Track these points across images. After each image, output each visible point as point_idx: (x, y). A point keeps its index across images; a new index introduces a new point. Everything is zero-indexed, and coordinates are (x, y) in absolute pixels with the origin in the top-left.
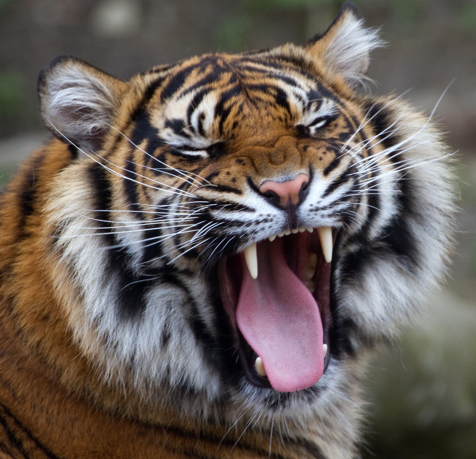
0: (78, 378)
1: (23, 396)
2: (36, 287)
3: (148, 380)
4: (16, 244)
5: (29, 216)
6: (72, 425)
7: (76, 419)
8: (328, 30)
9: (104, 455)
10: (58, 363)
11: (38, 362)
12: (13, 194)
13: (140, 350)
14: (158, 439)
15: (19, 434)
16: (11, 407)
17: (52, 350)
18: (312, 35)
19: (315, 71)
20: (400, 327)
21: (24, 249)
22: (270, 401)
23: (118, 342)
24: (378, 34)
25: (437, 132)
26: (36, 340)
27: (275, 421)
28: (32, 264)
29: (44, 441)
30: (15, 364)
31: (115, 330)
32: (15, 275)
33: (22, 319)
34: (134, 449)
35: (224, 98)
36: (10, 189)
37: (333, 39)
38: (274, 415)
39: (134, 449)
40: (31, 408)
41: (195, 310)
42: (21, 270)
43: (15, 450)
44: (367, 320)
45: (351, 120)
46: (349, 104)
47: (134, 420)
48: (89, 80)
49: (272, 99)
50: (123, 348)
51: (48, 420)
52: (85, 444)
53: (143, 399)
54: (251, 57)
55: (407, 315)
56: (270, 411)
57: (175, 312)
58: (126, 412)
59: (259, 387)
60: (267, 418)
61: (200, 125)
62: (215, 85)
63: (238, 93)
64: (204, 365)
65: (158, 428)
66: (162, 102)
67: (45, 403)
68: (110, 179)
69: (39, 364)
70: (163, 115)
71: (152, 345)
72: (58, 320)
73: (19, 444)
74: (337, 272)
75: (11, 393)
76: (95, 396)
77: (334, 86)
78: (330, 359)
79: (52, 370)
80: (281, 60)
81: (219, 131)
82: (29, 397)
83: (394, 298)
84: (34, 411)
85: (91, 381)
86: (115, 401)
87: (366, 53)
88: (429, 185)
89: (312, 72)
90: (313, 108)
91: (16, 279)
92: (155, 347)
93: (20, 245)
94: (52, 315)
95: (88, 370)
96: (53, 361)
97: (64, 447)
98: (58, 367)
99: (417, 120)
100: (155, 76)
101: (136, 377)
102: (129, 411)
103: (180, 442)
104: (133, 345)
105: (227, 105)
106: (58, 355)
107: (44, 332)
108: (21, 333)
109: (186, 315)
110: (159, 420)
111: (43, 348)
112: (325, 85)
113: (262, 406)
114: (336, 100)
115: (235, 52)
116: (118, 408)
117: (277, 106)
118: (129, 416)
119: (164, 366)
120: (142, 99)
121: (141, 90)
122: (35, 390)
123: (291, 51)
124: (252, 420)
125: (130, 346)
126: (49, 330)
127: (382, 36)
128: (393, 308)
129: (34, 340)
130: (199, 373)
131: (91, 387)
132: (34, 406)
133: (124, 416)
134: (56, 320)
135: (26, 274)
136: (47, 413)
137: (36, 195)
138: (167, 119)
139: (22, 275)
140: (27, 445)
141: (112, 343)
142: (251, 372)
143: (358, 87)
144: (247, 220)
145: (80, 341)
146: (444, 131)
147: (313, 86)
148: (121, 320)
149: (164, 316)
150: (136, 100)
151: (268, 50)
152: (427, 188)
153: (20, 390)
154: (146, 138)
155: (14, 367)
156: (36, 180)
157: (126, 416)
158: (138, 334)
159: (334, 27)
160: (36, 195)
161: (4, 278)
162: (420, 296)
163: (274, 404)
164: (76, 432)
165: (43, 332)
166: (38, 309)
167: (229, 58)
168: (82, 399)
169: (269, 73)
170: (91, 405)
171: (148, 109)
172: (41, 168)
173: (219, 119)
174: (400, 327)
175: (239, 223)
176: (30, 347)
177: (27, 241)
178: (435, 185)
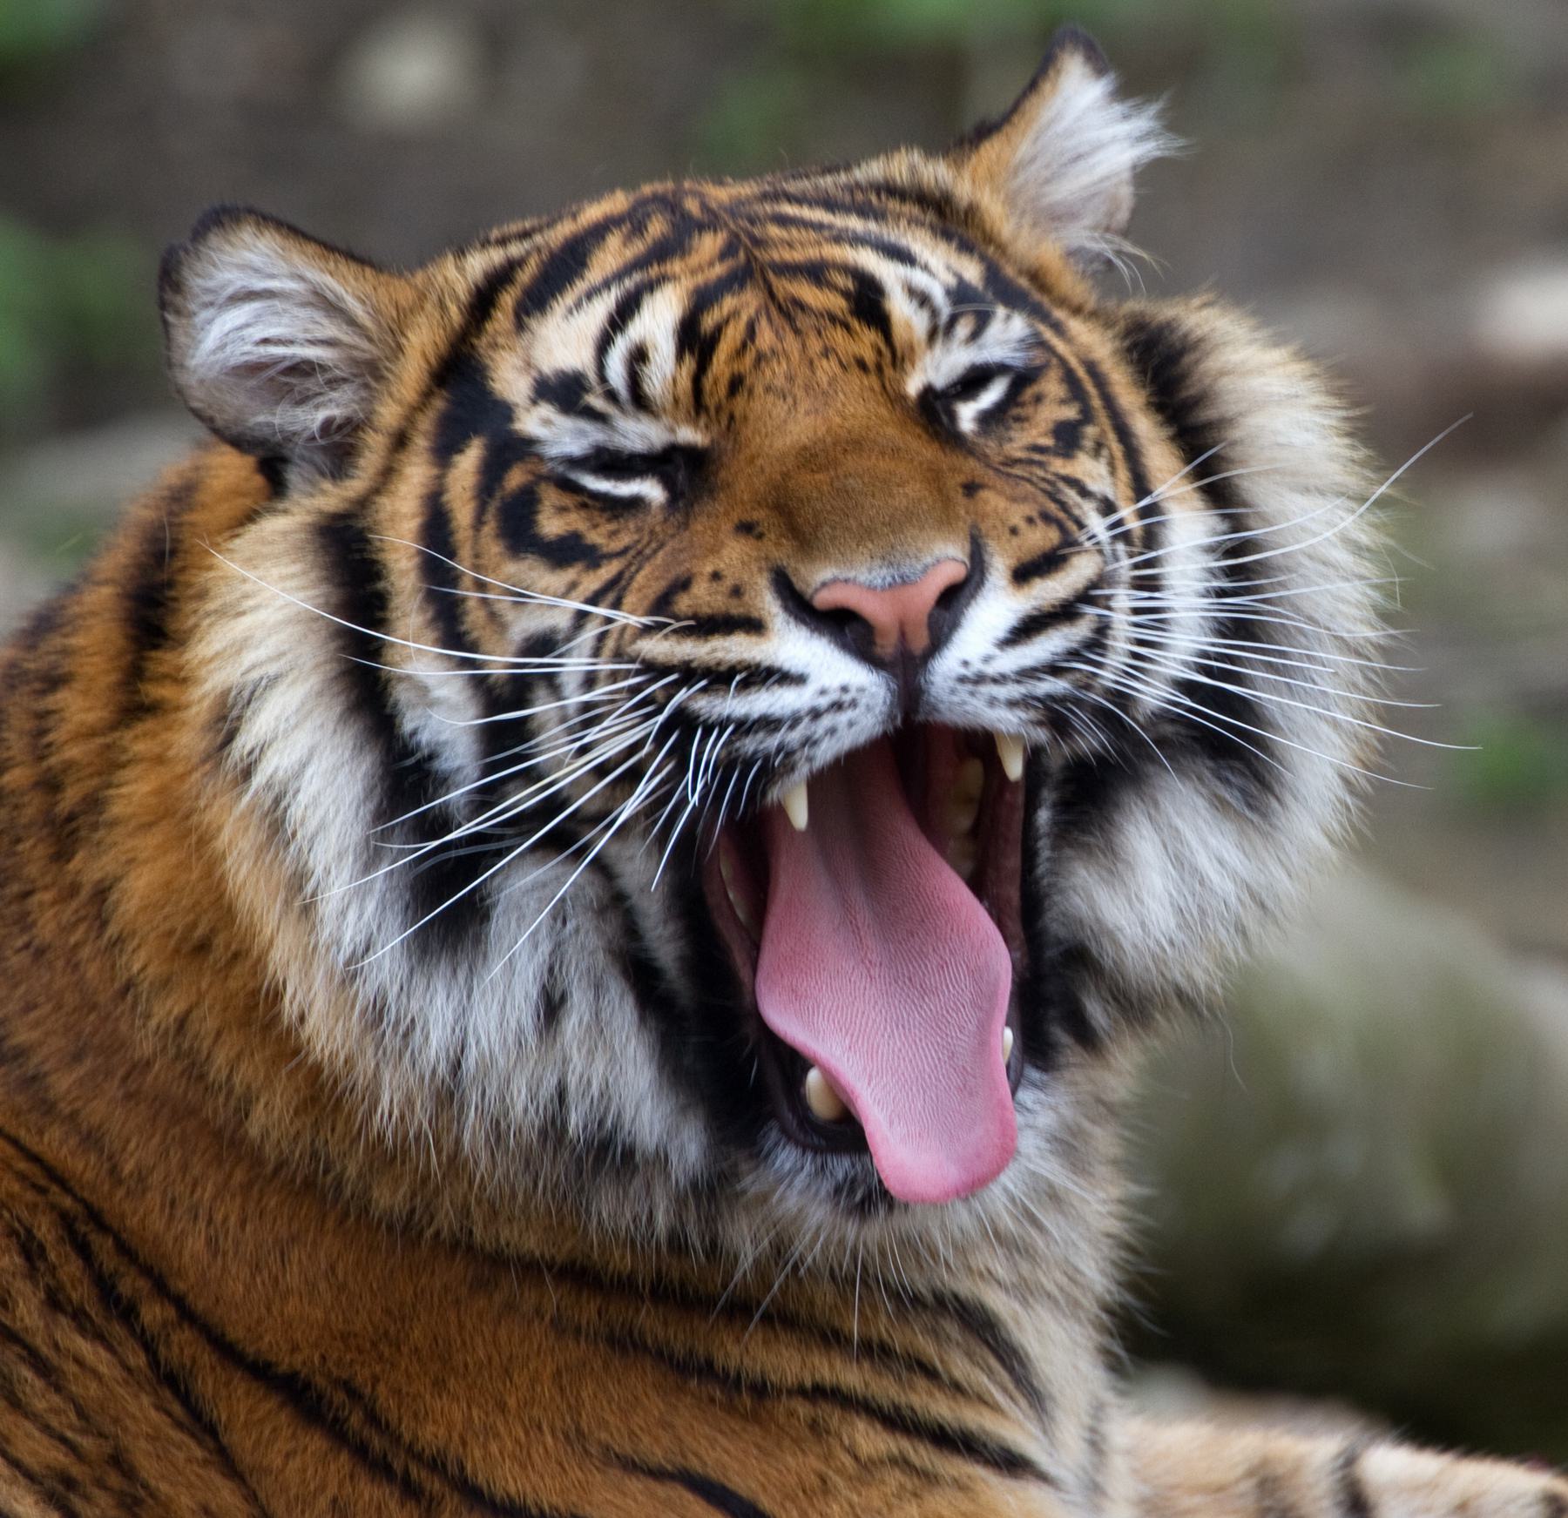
0: (298, 1124)
1: (140, 1173)
2: (172, 858)
3: (503, 1125)
4: (117, 734)
5: (153, 654)
6: (282, 1254)
7: (293, 1239)
8: (1015, 107)
9: (374, 1344)
10: (237, 1080)
11: (182, 1073)
12: (106, 591)
13: (478, 1043)
14: (529, 1299)
15: (130, 1284)
16: (106, 1206)
17: (221, 1041)
18: (968, 124)
19: (984, 231)
20: (1224, 963)
21: (140, 747)
22: (852, 1191)
23: (413, 1020)
24: (1160, 116)
25: (1335, 408)
26: (176, 1011)
27: (865, 1244)
28: (162, 791)
29: (200, 1305)
30: (116, 1082)
31: (405, 988)
32: (113, 824)
33: (134, 951)
34: (461, 1327)
35: (701, 301)
36: (102, 576)
37: (1031, 135)
38: (863, 1233)
39: (461, 1327)
40: (163, 1206)
41: (631, 929)
42: (129, 810)
43: (117, 1330)
44: (1127, 946)
45: (1081, 373)
46: (1076, 326)
47: (460, 1246)
49: (838, 304)
50: (427, 1038)
51: (212, 1244)
52: (319, 1314)
53: (482, 1178)
54: (793, 187)
55: (1242, 931)
56: (850, 1224)
57: (577, 931)
58: (436, 1221)
59: (816, 1151)
60: (841, 1242)
61: (635, 381)
62: (676, 266)
63: (742, 286)
64: (661, 1086)
65: (530, 1268)
66: (520, 326)
67: (203, 1194)
68: (381, 556)
69: (184, 1081)
70: (529, 364)
71: (513, 1024)
72: (236, 956)
73: (128, 1313)
74: (1044, 816)
75: (106, 1166)
76: (348, 1174)
77: (1037, 277)
78: (1022, 1068)
79: (221, 1100)
80: (883, 197)
81: (691, 399)
82: (156, 1178)
83: (1202, 883)
84: (171, 1217)
85: (333, 1130)
86: (401, 1192)
87: (1126, 175)
88: (1306, 562)
89: (971, 234)
90: (963, 329)
91: (118, 833)
92: (521, 1031)
93: (126, 736)
94: (219, 941)
95: (324, 1100)
96: (224, 1074)
97: (259, 1322)
98: (239, 1090)
99: (1281, 370)
100: (496, 256)
101: (467, 1116)
102: (446, 1218)
103: (593, 1307)
104: (457, 1030)
105: (709, 321)
106: (239, 1056)
107: (199, 989)
108: (132, 990)
109: (610, 942)
110: (532, 1243)
111: (196, 1036)
112: (1009, 271)
113: (828, 1207)
114: (1037, 312)
115: (742, 175)
116: (412, 1211)
117: (855, 324)
118: (445, 1233)
119: (550, 1083)
120: (461, 326)
121: (458, 299)
122: (175, 1157)
123: (913, 169)
124: (799, 1247)
125: (449, 1030)
126: (210, 985)
127: (1172, 123)
128: (1202, 911)
129: (170, 1012)
130: (647, 1107)
131: (333, 1150)
132: (173, 1204)
133: (429, 1233)
134: (229, 954)
135: (146, 819)
136: (210, 1221)
137: (173, 593)
138: (540, 372)
139: (133, 824)
140: (153, 1313)
141: (397, 1022)
142: (793, 1110)
143: (1104, 271)
144: (787, 711)
145: (302, 1019)
146: (1355, 404)
147: (972, 272)
148: (421, 960)
149: (547, 941)
150: (445, 330)
151: (848, 168)
152: (1302, 571)
153: (132, 1155)
154: (476, 432)
155: (113, 1089)
156: (173, 552)
157: (437, 1234)
158: (469, 997)
159: (1034, 100)
160: (173, 593)
161: (83, 833)
162: (1283, 884)
163: (862, 1202)
164: (293, 1278)
165: (194, 989)
166: (180, 924)
167: (720, 195)
168: (309, 1184)
169: (834, 233)
170: (336, 1200)
171: (482, 351)
172: (187, 518)
173: (690, 363)
174: (1224, 963)
175: (769, 724)
176: (156, 1033)
177: (149, 724)
178: (1325, 563)
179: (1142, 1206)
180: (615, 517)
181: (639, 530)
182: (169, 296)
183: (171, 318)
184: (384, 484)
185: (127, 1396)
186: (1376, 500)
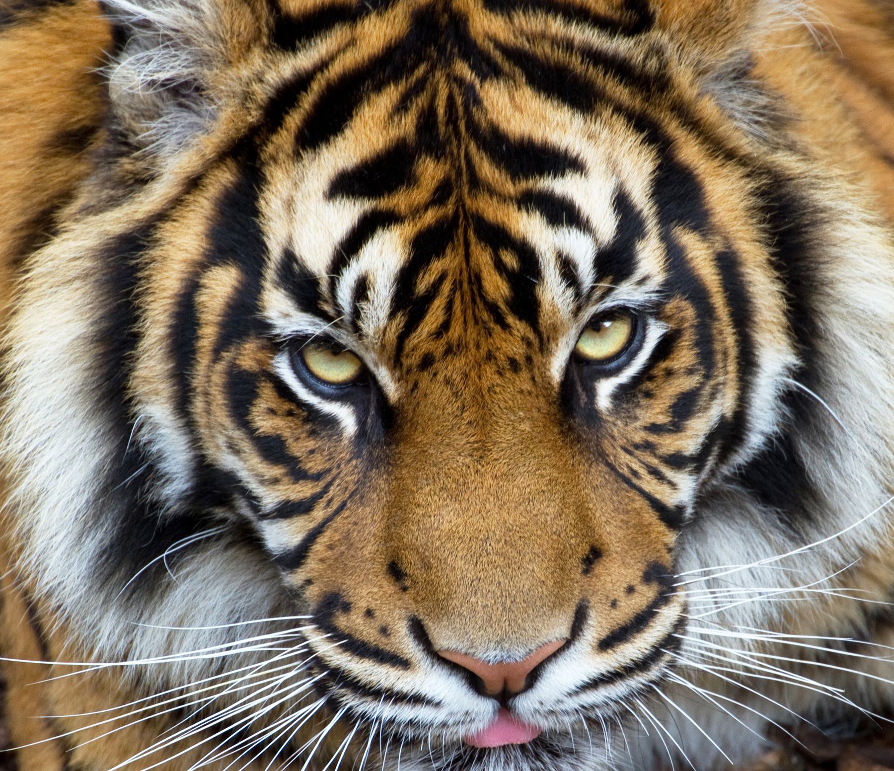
62: (400, 201)
66: (297, 156)
68: (366, 58)
173: (400, 320)
179: (704, 205)
180: (312, 433)
184: (197, 275)
185: (66, 644)
186: (846, 587)
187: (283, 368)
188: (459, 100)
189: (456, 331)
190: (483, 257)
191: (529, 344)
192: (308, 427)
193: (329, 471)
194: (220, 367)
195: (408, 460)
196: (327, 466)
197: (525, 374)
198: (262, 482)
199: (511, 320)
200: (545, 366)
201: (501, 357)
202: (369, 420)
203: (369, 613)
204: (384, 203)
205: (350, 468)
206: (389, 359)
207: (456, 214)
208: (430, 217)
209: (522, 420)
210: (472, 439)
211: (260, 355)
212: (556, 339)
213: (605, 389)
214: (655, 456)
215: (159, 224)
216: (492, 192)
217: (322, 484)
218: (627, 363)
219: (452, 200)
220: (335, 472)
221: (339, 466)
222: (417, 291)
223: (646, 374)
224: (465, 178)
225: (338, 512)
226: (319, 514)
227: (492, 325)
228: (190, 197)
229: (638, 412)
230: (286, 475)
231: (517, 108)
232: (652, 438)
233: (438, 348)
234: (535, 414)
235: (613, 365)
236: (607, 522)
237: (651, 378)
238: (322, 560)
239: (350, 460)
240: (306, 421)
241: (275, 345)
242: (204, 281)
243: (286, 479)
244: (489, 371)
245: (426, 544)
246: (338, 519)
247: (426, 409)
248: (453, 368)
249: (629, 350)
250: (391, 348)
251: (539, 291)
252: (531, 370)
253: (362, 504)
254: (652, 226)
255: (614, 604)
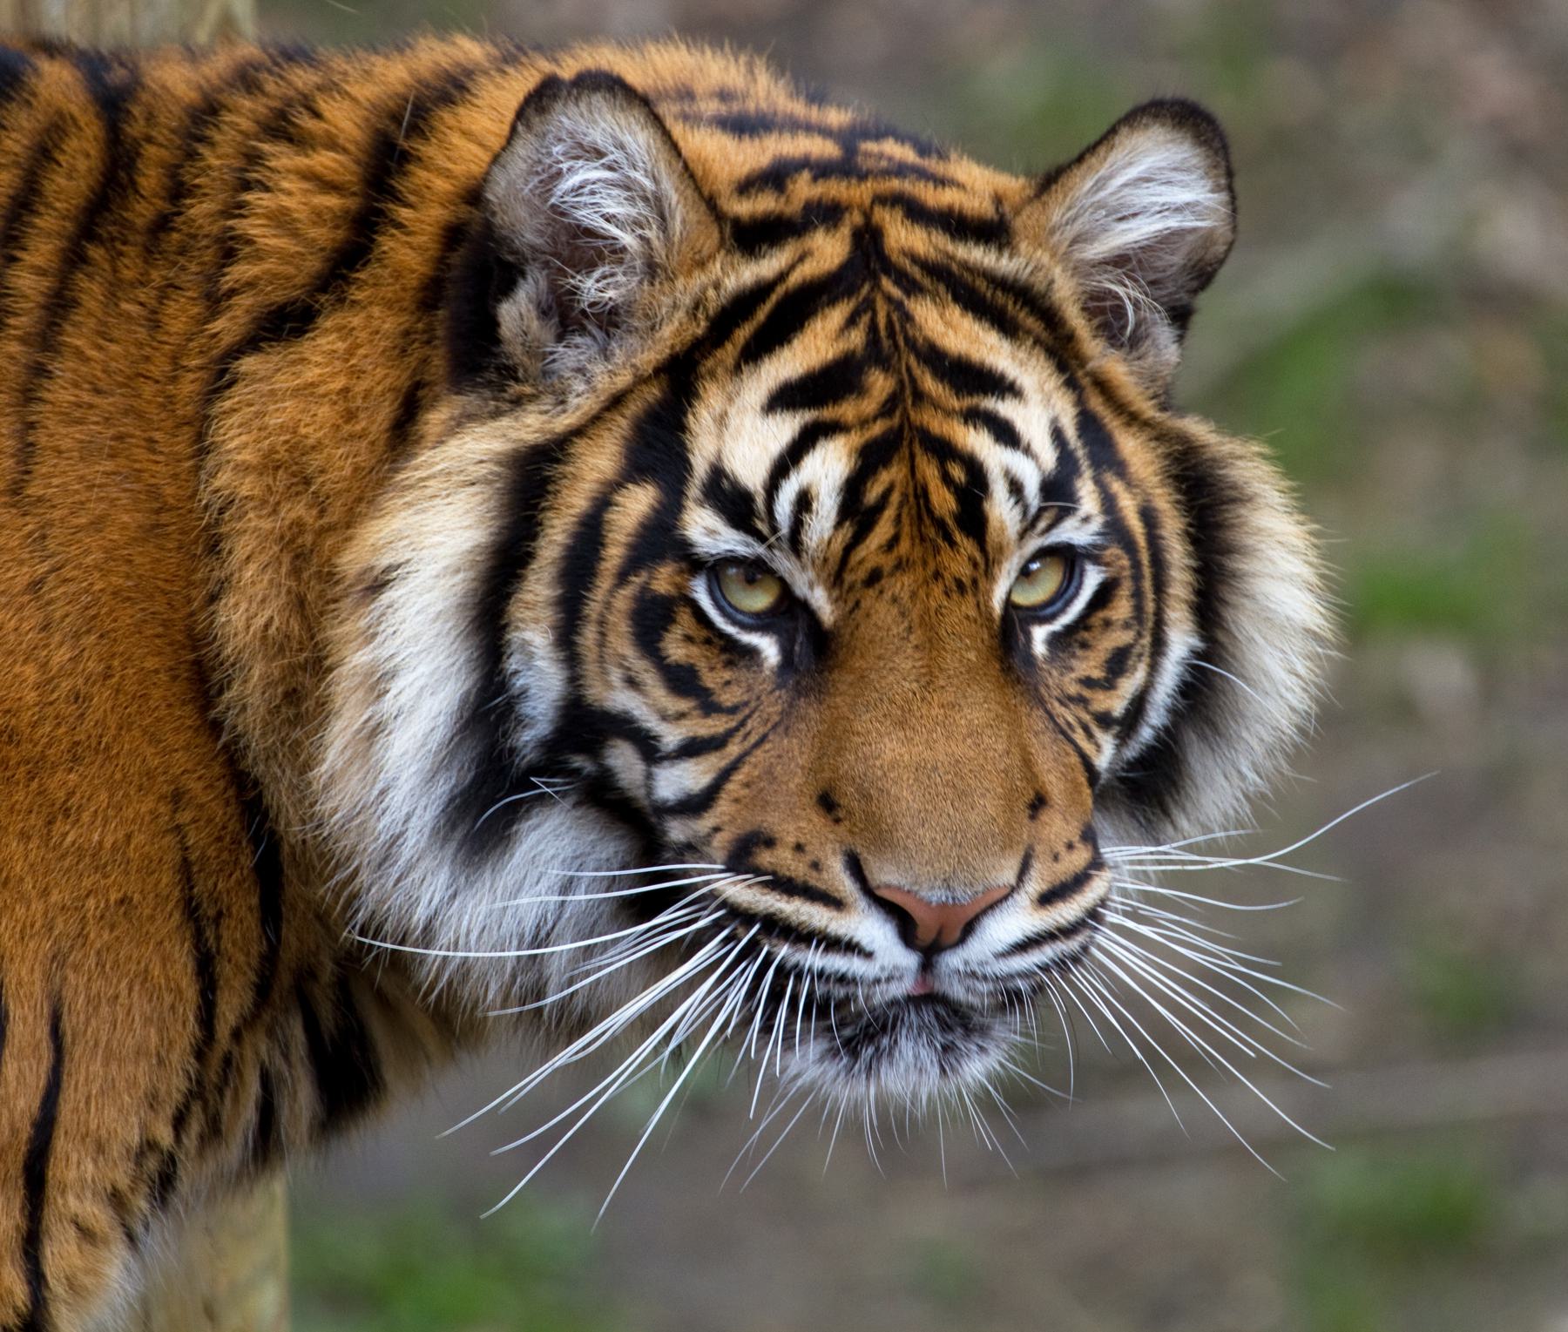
48: (656, 180)
61: (797, 525)
62: (847, 410)
66: (737, 370)
173: (847, 531)
180: (729, 664)
181: (750, 689)
182: (530, 111)
183: (520, 128)
187: (701, 593)
188: (895, 317)
189: (904, 546)
190: (929, 471)
191: (975, 565)
192: (724, 657)
193: (746, 704)
194: (627, 592)
195: (843, 688)
196: (745, 698)
197: (970, 598)
198: (665, 718)
199: (958, 537)
200: (988, 593)
201: (947, 575)
202: (797, 648)
203: (799, 848)
204: (828, 413)
205: (772, 698)
206: (829, 575)
207: (901, 427)
208: (877, 429)
209: (968, 649)
210: (918, 664)
211: (678, 579)
212: (1000, 563)
213: (1040, 635)
214: (1088, 712)
215: (575, 440)
216: (936, 406)
217: (739, 716)
218: (1062, 610)
219: (898, 414)
220: (753, 704)
221: (758, 698)
222: (865, 501)
223: (1082, 622)
224: (908, 392)
225: (757, 745)
226: (734, 749)
227: (940, 541)
228: (607, 415)
229: (1074, 663)
230: (695, 708)
231: (948, 324)
232: (1087, 693)
233: (887, 562)
234: (980, 645)
235: (1049, 611)
236: (1049, 771)
237: (1088, 628)
238: (737, 801)
239: (772, 692)
240: (724, 650)
241: (694, 563)
242: (618, 499)
243: (695, 713)
244: (937, 590)
245: (865, 775)
246: (759, 752)
247: (866, 631)
248: (901, 585)
249: (1063, 596)
250: (833, 564)
251: (987, 506)
252: (975, 595)
253: (787, 735)
254: (1084, 464)
255: (1056, 858)
